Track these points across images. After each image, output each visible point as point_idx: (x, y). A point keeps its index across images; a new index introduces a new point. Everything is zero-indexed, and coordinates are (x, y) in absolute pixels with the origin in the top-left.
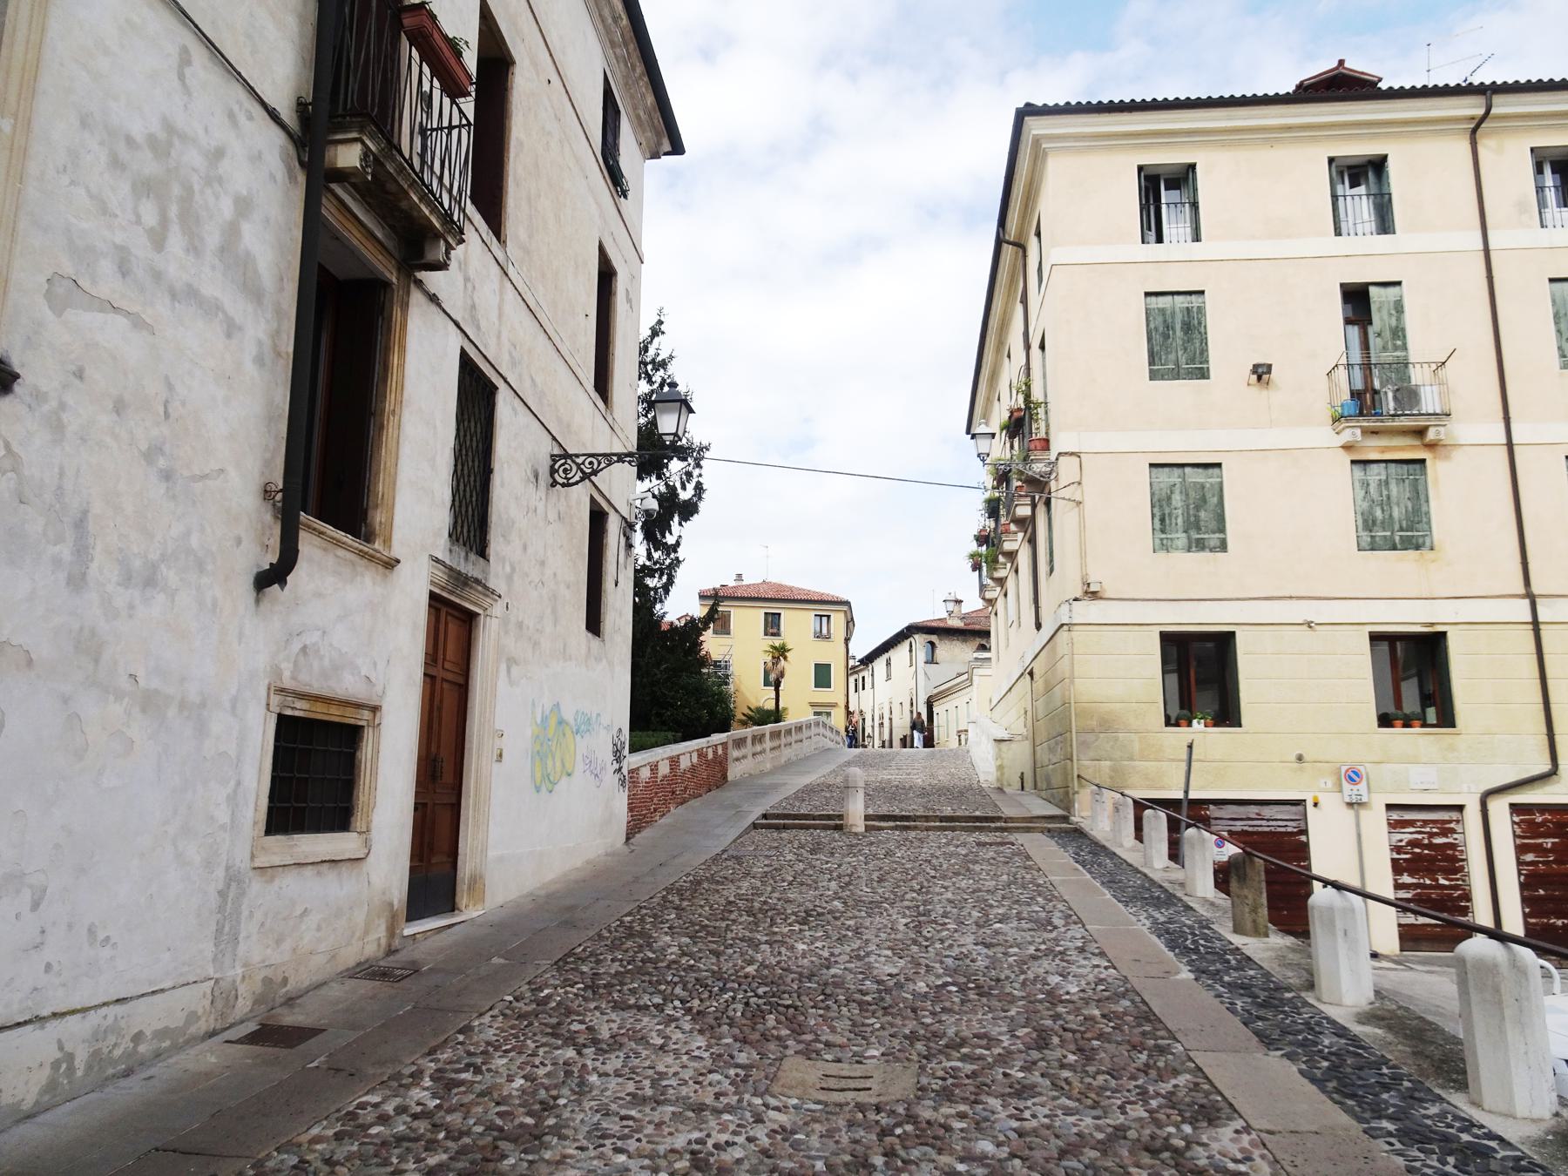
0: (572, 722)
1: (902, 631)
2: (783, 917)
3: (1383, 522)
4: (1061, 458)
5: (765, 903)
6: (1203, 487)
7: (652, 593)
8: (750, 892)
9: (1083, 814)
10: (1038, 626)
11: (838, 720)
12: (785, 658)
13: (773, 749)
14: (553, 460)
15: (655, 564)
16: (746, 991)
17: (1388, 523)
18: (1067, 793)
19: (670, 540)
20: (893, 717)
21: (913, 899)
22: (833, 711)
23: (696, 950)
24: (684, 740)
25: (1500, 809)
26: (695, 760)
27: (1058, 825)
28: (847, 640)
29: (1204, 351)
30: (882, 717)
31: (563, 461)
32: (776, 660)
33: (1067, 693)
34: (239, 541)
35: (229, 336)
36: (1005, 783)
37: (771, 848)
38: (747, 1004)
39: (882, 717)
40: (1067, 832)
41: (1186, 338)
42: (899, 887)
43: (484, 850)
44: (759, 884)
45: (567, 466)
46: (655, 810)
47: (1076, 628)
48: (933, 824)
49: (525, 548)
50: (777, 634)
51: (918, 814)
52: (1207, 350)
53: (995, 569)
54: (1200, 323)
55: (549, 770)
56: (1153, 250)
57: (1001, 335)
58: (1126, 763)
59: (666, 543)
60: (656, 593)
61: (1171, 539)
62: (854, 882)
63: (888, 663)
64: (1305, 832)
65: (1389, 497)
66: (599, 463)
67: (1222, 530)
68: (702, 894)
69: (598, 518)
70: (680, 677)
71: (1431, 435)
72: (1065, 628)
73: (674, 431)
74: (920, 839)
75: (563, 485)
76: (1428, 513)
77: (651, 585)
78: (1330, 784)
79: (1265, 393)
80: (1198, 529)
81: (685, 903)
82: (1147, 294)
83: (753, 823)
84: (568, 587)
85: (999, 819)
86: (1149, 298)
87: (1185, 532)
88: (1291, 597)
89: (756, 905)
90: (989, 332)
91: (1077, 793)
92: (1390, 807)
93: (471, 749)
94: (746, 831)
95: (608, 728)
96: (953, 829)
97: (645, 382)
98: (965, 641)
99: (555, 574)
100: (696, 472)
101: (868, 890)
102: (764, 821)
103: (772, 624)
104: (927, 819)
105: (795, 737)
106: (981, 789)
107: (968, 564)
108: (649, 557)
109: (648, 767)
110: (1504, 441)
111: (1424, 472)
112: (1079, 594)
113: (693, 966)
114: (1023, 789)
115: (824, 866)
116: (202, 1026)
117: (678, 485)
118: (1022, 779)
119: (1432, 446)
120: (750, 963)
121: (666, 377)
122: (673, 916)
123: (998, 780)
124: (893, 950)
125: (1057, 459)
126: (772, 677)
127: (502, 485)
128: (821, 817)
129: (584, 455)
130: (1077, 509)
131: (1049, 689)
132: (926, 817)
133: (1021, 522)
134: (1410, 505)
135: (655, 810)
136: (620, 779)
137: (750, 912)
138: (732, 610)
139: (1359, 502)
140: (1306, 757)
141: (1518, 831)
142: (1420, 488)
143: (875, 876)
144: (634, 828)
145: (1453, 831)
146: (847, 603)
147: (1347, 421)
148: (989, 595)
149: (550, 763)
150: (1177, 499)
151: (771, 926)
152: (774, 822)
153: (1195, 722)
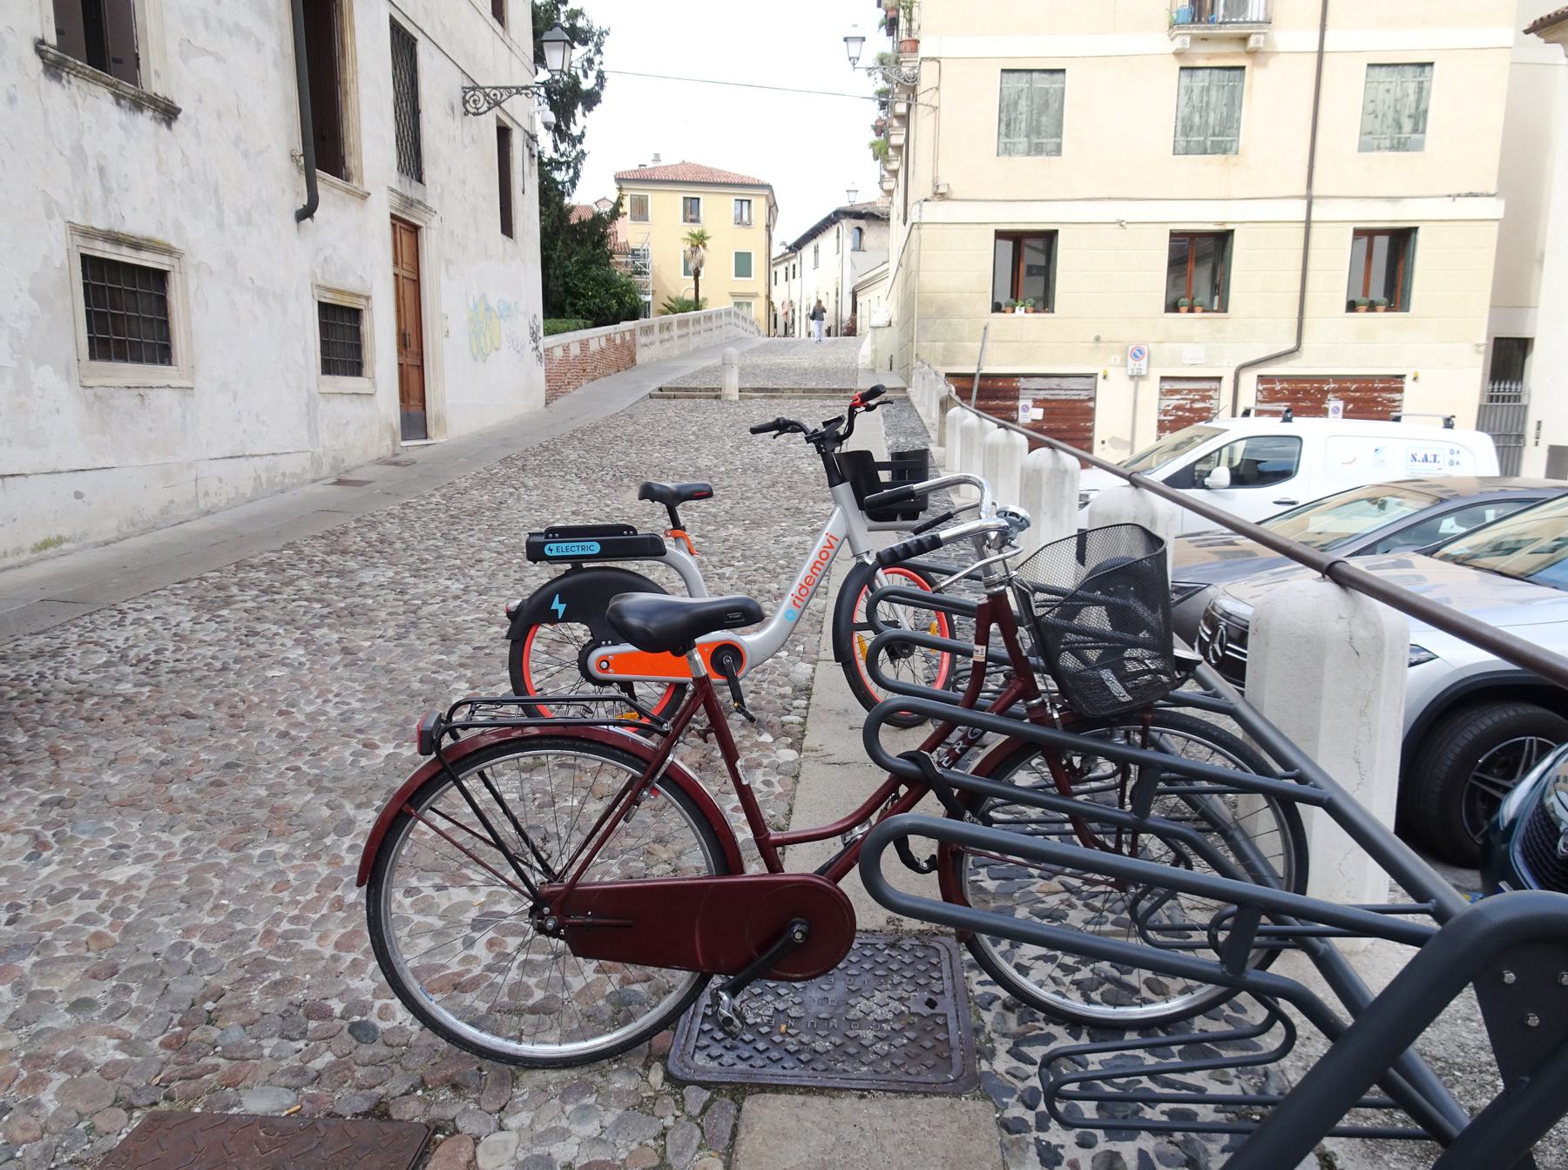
3: (1199, 128)
6: (1047, 92)
11: (758, 310)
12: (704, 246)
13: (680, 337)
17: (1203, 129)
22: (754, 302)
24: (596, 325)
25: (1249, 381)
26: (603, 343)
32: (695, 247)
34: (284, 191)
35: (259, 51)
49: (449, 171)
53: (888, 161)
63: (816, 251)
64: (1092, 399)
65: (1208, 104)
67: (1059, 135)
69: (503, 133)
71: (1252, 43)
75: (474, 114)
76: (1239, 119)
78: (1118, 361)
80: (1039, 133)
84: (485, 199)
87: (1027, 136)
92: (1163, 379)
94: (642, 399)
100: (597, 59)
103: (691, 210)
104: (792, 390)
105: (703, 326)
108: (556, 149)
110: (1316, 48)
111: (1242, 79)
112: (929, 195)
116: (309, 476)
119: (1253, 53)
123: (872, 362)
126: (692, 266)
134: (1225, 110)
139: (1181, 107)
140: (1103, 338)
141: (1260, 397)
142: (1237, 94)
144: (553, 394)
145: (1210, 398)
146: (768, 187)
147: (1179, 28)
150: (1023, 104)
152: (665, 394)
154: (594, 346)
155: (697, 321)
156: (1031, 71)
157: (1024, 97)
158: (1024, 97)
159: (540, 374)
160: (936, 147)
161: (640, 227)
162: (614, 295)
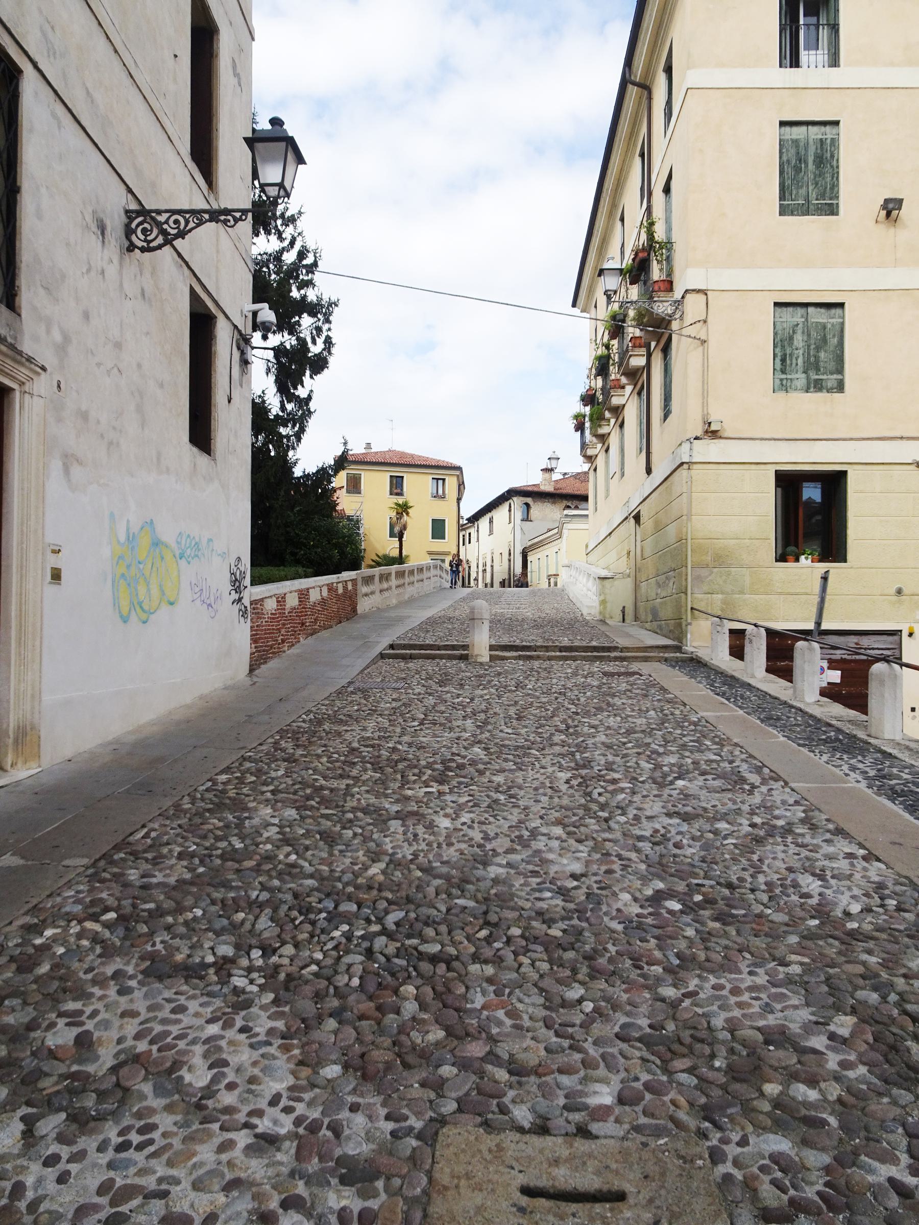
0: (174, 545)
1: (503, 494)
2: (416, 771)
4: (688, 296)
5: (394, 749)
6: (824, 327)
7: (285, 440)
8: (377, 734)
9: (695, 644)
10: (649, 471)
12: (407, 514)
13: (397, 587)
14: (129, 217)
15: (288, 415)
16: (368, 921)
18: (680, 625)
19: (302, 392)
20: (495, 564)
21: (563, 744)
23: (302, 832)
26: (325, 593)
27: (672, 655)
28: (459, 500)
29: (835, 186)
30: (485, 565)
31: (140, 219)
32: (400, 515)
33: (685, 529)
36: (607, 616)
37: (399, 679)
38: (369, 953)
39: (485, 565)
40: (683, 661)
41: (817, 172)
42: (542, 726)
43: (36, 696)
44: (387, 724)
45: (146, 225)
46: (283, 641)
47: (695, 466)
48: (553, 654)
49: (86, 316)
50: (400, 494)
51: (538, 644)
52: (838, 185)
53: (600, 426)
54: (832, 156)
55: (141, 597)
56: (790, 76)
57: (614, 198)
58: (737, 596)
59: (298, 396)
60: (288, 441)
61: (791, 379)
62: (492, 720)
63: (491, 521)
66: (187, 222)
67: (840, 370)
68: (321, 738)
70: (313, 519)
72: (685, 466)
73: (279, 180)
74: (545, 669)
75: (143, 250)
77: (284, 433)
79: (892, 230)
80: (817, 370)
81: (300, 752)
82: (783, 124)
83: (381, 653)
84: (161, 386)
85: (615, 649)
86: (783, 128)
87: (804, 372)
88: (902, 438)
89: (384, 753)
90: (604, 195)
91: (690, 624)
93: (9, 566)
94: (374, 662)
95: (223, 555)
96: (574, 659)
97: (276, 237)
98: (554, 503)
99: (139, 366)
100: (325, 327)
101: (510, 731)
102: (392, 651)
103: (397, 485)
104: (547, 649)
105: (416, 577)
106: (586, 623)
107: (572, 424)
108: (283, 408)
109: (274, 599)
112: (699, 433)
113: (293, 865)
114: (624, 620)
115: (457, 700)
117: (309, 340)
118: (623, 612)
120: (375, 857)
121: (296, 235)
122: (280, 773)
123: (600, 613)
124: (565, 826)
125: (683, 297)
127: (39, 216)
128: (446, 647)
129: (166, 211)
130: (701, 348)
131: (659, 527)
132: (546, 647)
133: (632, 374)
135: (283, 641)
136: (240, 610)
137: (377, 767)
138: (363, 473)
140: (905, 591)
143: (512, 711)
146: (459, 469)
148: (590, 452)
149: (142, 590)
151: (402, 787)
153: (802, 558)
154: (314, 596)
155: (400, 574)
156: (806, 305)
157: (799, 331)
158: (799, 331)
159: (242, 633)
160: (705, 382)
161: (354, 498)
162: (336, 546)
